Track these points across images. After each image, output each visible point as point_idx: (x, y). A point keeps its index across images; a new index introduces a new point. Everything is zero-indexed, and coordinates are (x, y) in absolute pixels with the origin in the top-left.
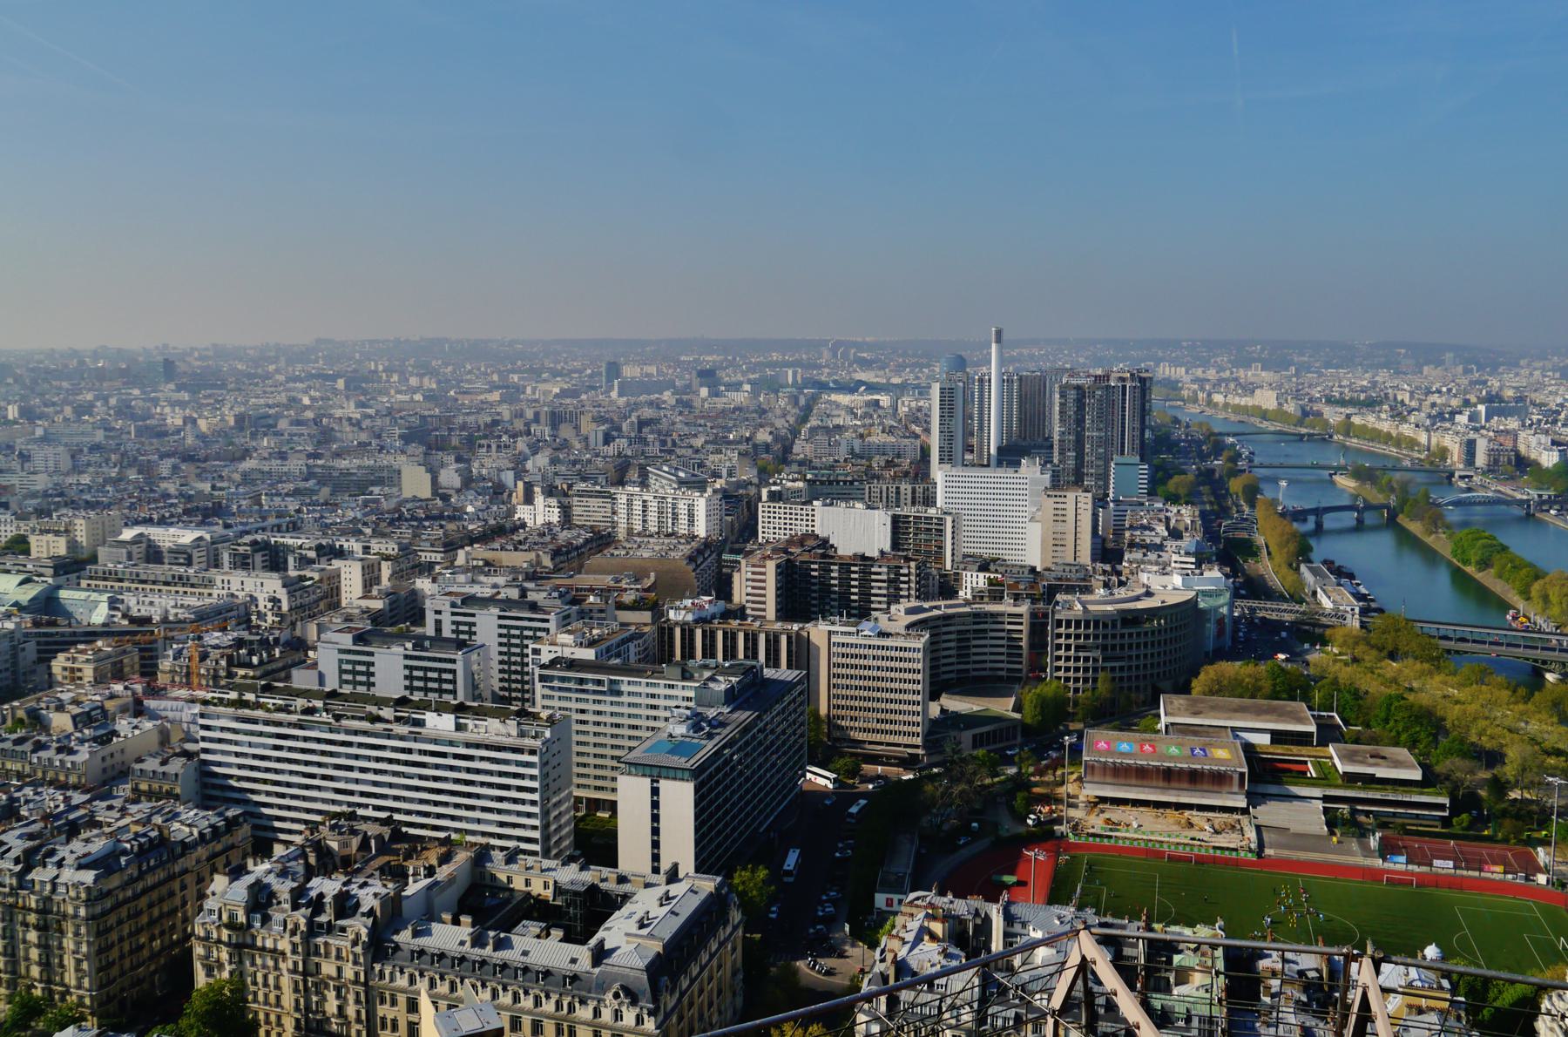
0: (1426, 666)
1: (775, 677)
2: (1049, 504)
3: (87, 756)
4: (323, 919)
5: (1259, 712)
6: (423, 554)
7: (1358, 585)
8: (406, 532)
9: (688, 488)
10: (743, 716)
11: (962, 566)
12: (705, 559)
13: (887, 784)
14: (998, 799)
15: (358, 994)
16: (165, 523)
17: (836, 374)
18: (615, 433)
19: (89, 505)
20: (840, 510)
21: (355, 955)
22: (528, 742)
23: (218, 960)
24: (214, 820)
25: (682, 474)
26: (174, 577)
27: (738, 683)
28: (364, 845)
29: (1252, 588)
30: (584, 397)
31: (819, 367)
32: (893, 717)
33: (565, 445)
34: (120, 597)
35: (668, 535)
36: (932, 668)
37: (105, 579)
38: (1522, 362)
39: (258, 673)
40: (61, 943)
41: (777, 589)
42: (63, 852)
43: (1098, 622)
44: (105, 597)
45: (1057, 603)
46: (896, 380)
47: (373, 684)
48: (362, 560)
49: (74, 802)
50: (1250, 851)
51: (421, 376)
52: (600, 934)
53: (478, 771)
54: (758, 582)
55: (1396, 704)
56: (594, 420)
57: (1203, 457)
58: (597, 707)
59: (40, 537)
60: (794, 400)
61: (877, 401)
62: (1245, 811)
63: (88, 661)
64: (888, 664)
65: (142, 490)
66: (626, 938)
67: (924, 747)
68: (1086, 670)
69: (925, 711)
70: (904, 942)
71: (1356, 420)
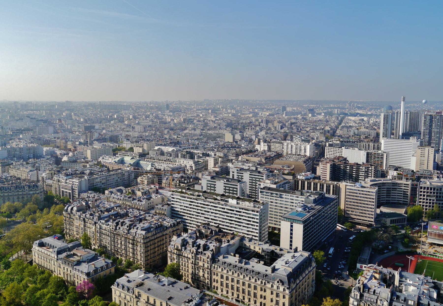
2: (419, 151)
9: (305, 142)
11: (389, 169)
12: (309, 162)
17: (350, 111)
18: (284, 126)
19: (148, 140)
23: (173, 258)
24: (174, 222)
25: (303, 138)
27: (317, 197)
28: (211, 232)
30: (275, 116)
31: (345, 109)
32: (365, 212)
33: (270, 129)
35: (298, 155)
37: (151, 159)
39: (186, 185)
42: (138, 226)
46: (369, 113)
49: (141, 214)
51: (231, 109)
52: (274, 264)
54: (324, 169)
63: (146, 179)
65: (160, 137)
69: (375, 211)
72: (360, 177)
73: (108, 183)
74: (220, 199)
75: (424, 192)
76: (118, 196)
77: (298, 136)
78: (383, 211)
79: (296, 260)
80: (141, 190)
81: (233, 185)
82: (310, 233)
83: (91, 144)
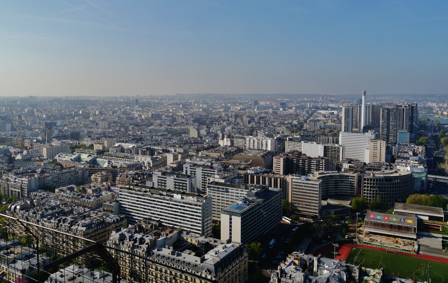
4: (136, 244)
5: (426, 210)
8: (187, 146)
10: (259, 200)
11: (343, 162)
13: (307, 223)
17: (323, 104)
18: (252, 121)
19: (110, 137)
20: (309, 144)
22: (199, 203)
24: (117, 218)
25: (266, 133)
26: (125, 156)
28: (152, 227)
30: (247, 110)
31: (318, 102)
32: (310, 204)
33: (238, 124)
37: (109, 156)
39: (140, 182)
42: (79, 222)
43: (379, 180)
45: (365, 173)
47: (166, 186)
48: (173, 153)
49: (86, 211)
50: (415, 251)
51: (203, 104)
53: (186, 210)
56: (247, 117)
57: (435, 131)
60: (308, 112)
61: (333, 113)
62: (416, 240)
63: (99, 176)
64: (309, 188)
65: (124, 133)
68: (373, 194)
69: (320, 203)
70: (285, 265)
72: (312, 171)
73: (60, 182)
74: (165, 195)
75: (368, 183)
76: (67, 194)
77: (262, 131)
78: (331, 203)
79: (226, 250)
81: (183, 180)
82: (250, 225)
83: (50, 141)
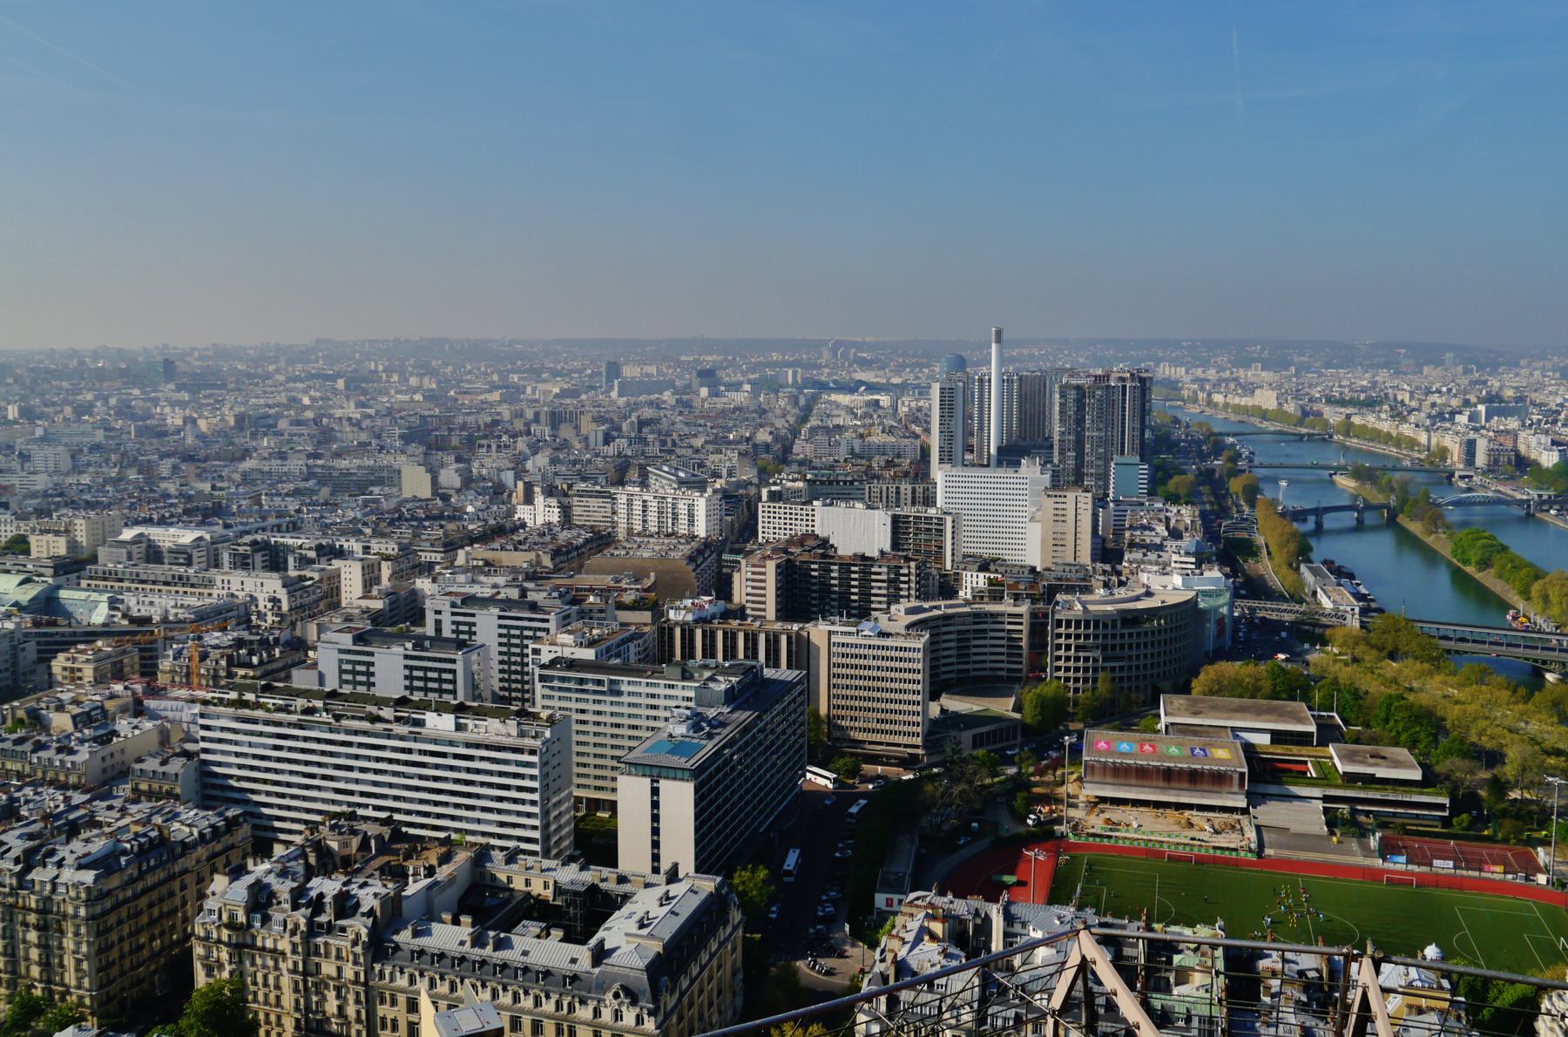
0: (1426, 666)
1: (775, 677)
2: (1049, 504)
3: (87, 756)
4: (323, 919)
5: (1259, 712)
6: (423, 554)
7: (1358, 585)
8: (406, 532)
9: (688, 488)
10: (743, 716)
11: (962, 566)
12: (705, 559)
13: (887, 784)
14: (998, 799)
15: (358, 994)
16: (165, 523)
17: (836, 374)
18: (615, 433)
19: (89, 505)
20: (840, 510)
21: (355, 955)
22: (528, 742)
23: (218, 960)
24: (214, 820)
25: (682, 474)
26: (174, 577)
27: (738, 683)
28: (364, 845)
29: (1252, 588)
30: (584, 397)
31: (819, 367)
32: (893, 717)
33: (565, 445)
34: (120, 597)
35: (668, 535)
36: (932, 668)
37: (105, 579)
38: (1522, 362)
39: (258, 673)
40: (61, 943)
41: (777, 589)
42: (63, 852)
43: (1098, 622)
44: (105, 597)
45: (1057, 603)
46: (896, 380)
47: (373, 684)
48: (362, 560)
49: (74, 802)
50: (1250, 851)
51: (421, 376)
52: (600, 934)
53: (478, 771)
54: (758, 582)
55: (1396, 704)
56: (594, 420)
57: (1203, 457)
58: (597, 707)
59: (40, 537)
60: (794, 400)
61: (877, 401)
62: (1245, 811)
63: (88, 661)
64: (888, 664)
65: (142, 490)
66: (626, 938)
67: (924, 747)
68: (1086, 670)
69: (925, 711)
71: (1356, 420)
80: (70, 707)
